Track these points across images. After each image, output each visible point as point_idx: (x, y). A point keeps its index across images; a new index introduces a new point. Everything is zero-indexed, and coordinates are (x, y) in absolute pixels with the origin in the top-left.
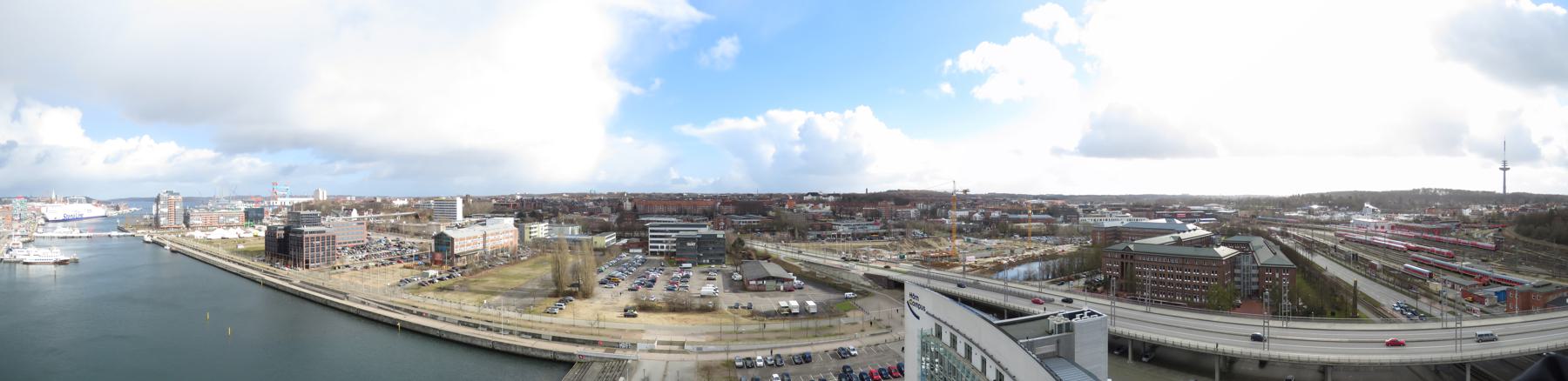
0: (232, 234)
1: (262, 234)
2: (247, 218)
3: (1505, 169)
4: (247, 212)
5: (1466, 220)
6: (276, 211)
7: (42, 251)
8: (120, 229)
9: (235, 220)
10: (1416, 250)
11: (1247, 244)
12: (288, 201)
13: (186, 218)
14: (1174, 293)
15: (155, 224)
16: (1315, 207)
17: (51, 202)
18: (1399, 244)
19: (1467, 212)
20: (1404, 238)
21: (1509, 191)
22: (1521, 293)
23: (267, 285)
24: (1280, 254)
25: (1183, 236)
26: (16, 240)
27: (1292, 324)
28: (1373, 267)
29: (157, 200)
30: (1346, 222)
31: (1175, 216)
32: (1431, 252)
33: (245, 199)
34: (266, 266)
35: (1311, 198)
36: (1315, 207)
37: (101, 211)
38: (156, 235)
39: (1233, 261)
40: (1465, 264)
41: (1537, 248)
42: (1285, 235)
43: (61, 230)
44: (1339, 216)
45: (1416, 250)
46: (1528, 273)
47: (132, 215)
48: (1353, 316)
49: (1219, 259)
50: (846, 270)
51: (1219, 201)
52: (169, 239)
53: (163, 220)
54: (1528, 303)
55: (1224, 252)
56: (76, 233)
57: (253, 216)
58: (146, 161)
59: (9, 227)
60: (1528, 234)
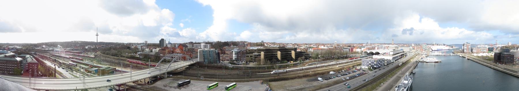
0: (485, 55)
1: (493, 55)
2: (489, 50)
3: (97, 35)
4: (489, 49)
5: (86, 50)
6: (497, 48)
7: (431, 59)
8: (453, 53)
9: (485, 51)
10: (72, 58)
11: (25, 57)
12: (500, 46)
13: (472, 50)
14: (10, 71)
15: (463, 52)
16: (44, 46)
17: (433, 45)
18: (68, 57)
19: (87, 47)
20: (69, 55)
21: (98, 41)
22: (102, 70)
23: (494, 69)
24: (34, 59)
25: (7, 55)
26: (424, 56)
27: (37, 79)
28: (60, 63)
29: (464, 45)
30: (53, 50)
31: (5, 49)
32: (76, 59)
33: (488, 45)
34: (495, 64)
35: (43, 44)
36: (44, 46)
37: (448, 48)
38: (463, 55)
39: (21, 61)
40: (86, 62)
41: (106, 57)
42: (36, 54)
43: (436, 53)
44: (51, 49)
45: (72, 58)
46: (104, 64)
47: (457, 49)
48: (55, 77)
49: (17, 61)
50: (112, 63)
51: (17, 45)
52: (467, 56)
53: (465, 51)
54: (104, 73)
55: (18, 59)
56: (441, 54)
57: (490, 50)
58: (455, 34)
59: (422, 52)
60: (104, 53)
